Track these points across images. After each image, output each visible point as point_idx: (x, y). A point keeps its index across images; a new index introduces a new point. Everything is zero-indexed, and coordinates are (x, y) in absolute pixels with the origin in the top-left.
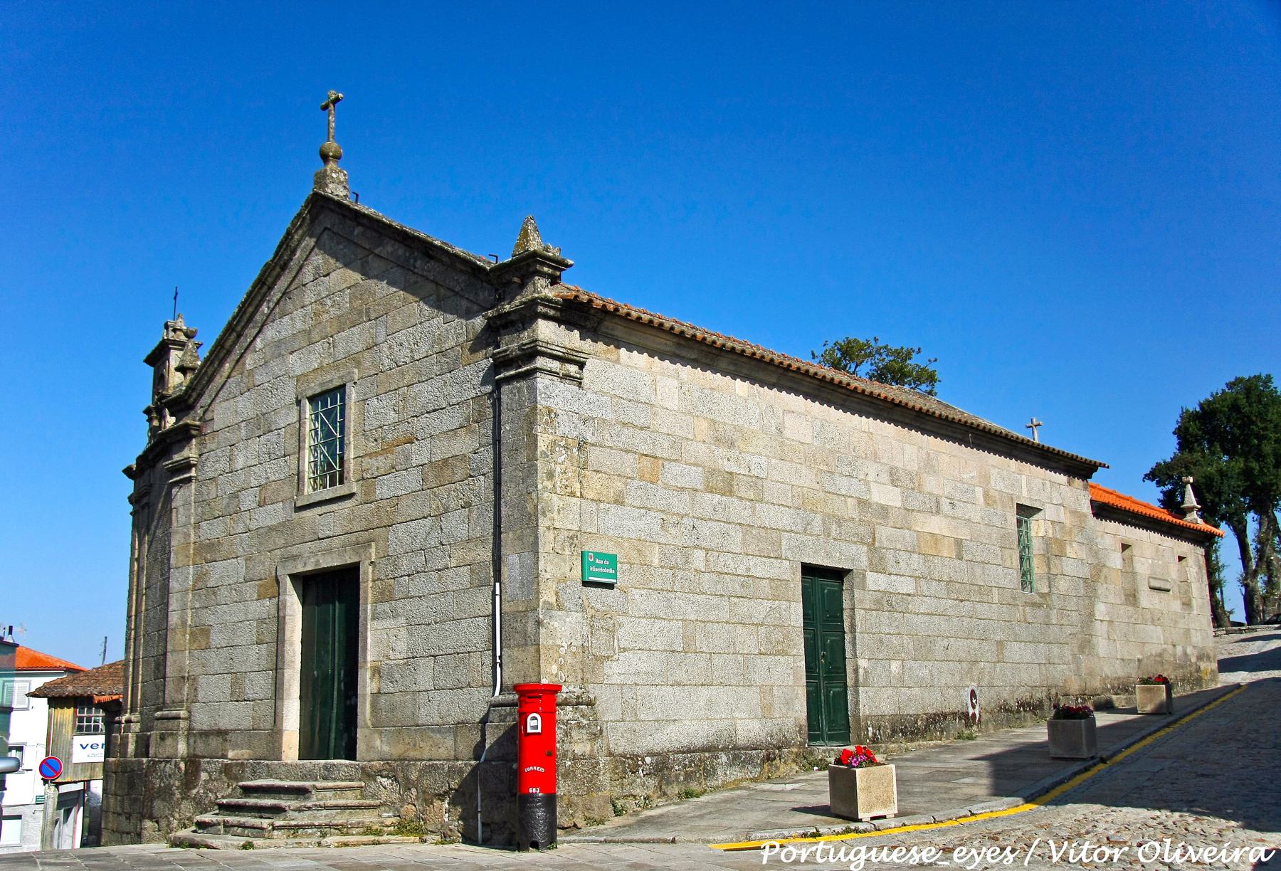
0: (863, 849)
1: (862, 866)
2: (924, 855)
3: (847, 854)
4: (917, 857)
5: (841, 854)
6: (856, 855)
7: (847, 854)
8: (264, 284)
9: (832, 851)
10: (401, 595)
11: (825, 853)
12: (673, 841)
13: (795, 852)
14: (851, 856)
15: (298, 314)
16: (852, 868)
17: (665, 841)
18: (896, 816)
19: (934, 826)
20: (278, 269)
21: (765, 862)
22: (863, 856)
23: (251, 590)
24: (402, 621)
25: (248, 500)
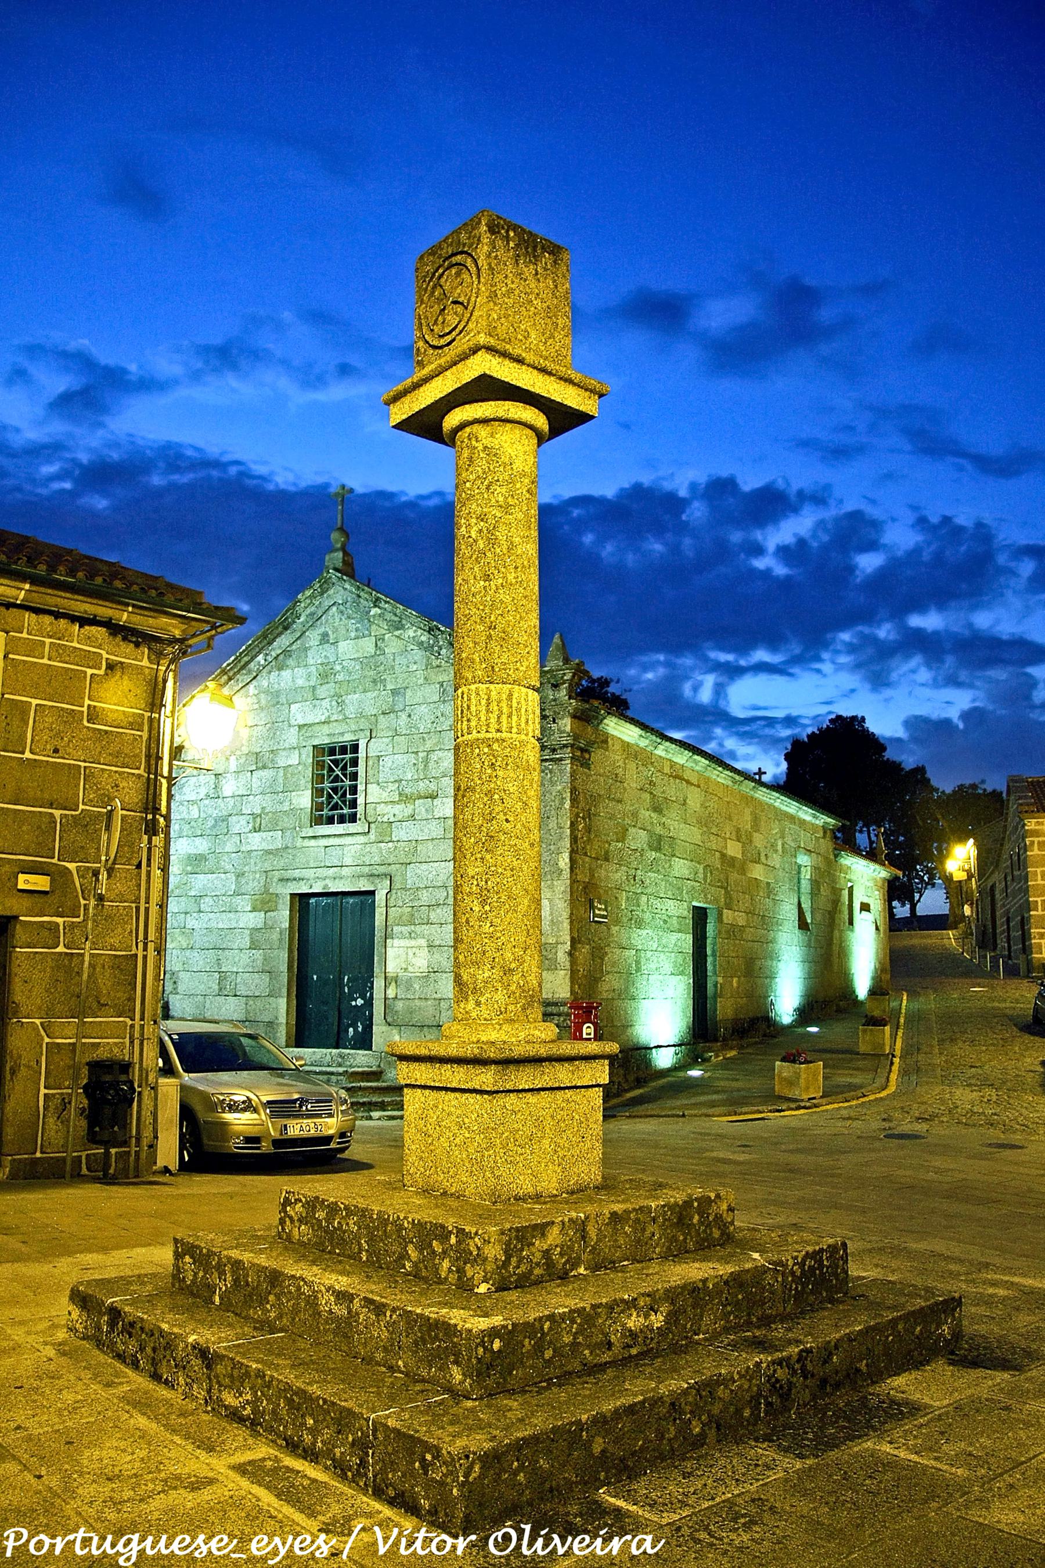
0: (136, 1537)
1: (133, 1559)
2: (214, 1544)
3: (113, 1545)
4: (204, 1549)
5: (107, 1544)
6: (125, 1546)
7: (113, 1545)
8: (265, 638)
9: (96, 1539)
10: (420, 921)
11: (86, 1542)
12: (684, 1116)
13: (47, 1541)
14: (120, 1547)
15: (300, 671)
16: (121, 1561)
17: (678, 1116)
18: (821, 1097)
19: (846, 1104)
20: (280, 629)
21: (9, 1554)
22: (134, 1546)
23: (244, 903)
24: (423, 942)
25: (240, 824)
